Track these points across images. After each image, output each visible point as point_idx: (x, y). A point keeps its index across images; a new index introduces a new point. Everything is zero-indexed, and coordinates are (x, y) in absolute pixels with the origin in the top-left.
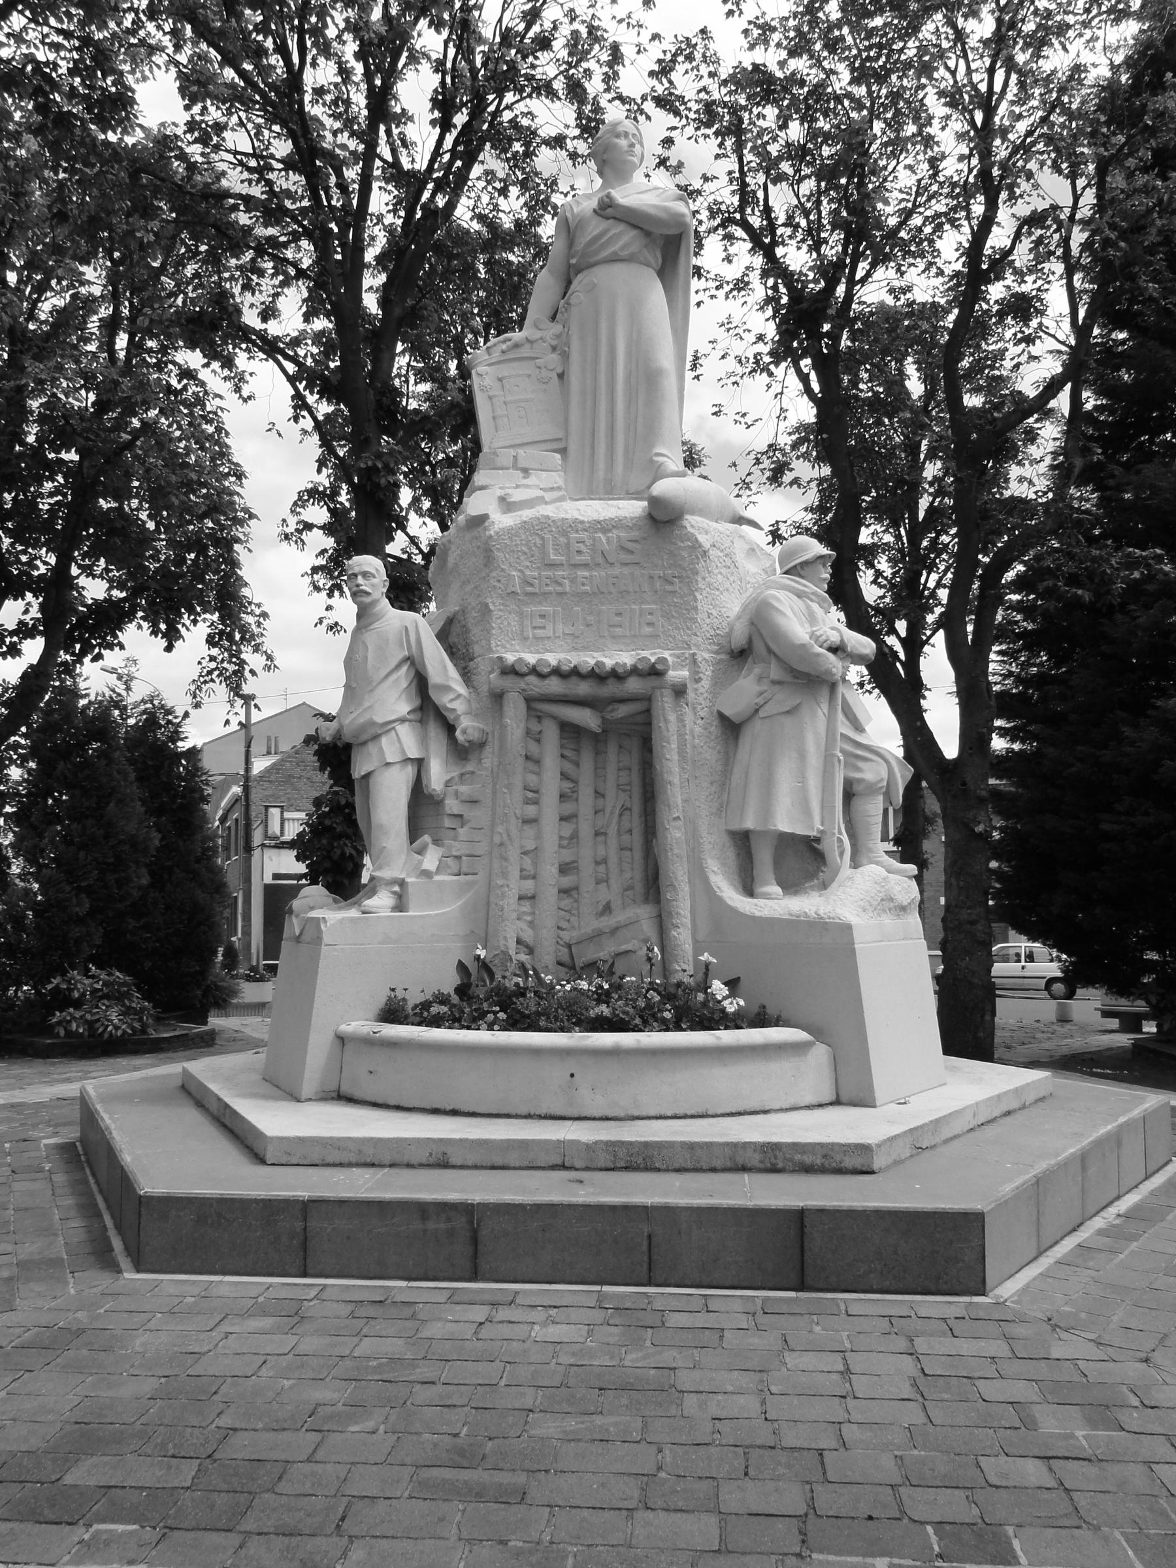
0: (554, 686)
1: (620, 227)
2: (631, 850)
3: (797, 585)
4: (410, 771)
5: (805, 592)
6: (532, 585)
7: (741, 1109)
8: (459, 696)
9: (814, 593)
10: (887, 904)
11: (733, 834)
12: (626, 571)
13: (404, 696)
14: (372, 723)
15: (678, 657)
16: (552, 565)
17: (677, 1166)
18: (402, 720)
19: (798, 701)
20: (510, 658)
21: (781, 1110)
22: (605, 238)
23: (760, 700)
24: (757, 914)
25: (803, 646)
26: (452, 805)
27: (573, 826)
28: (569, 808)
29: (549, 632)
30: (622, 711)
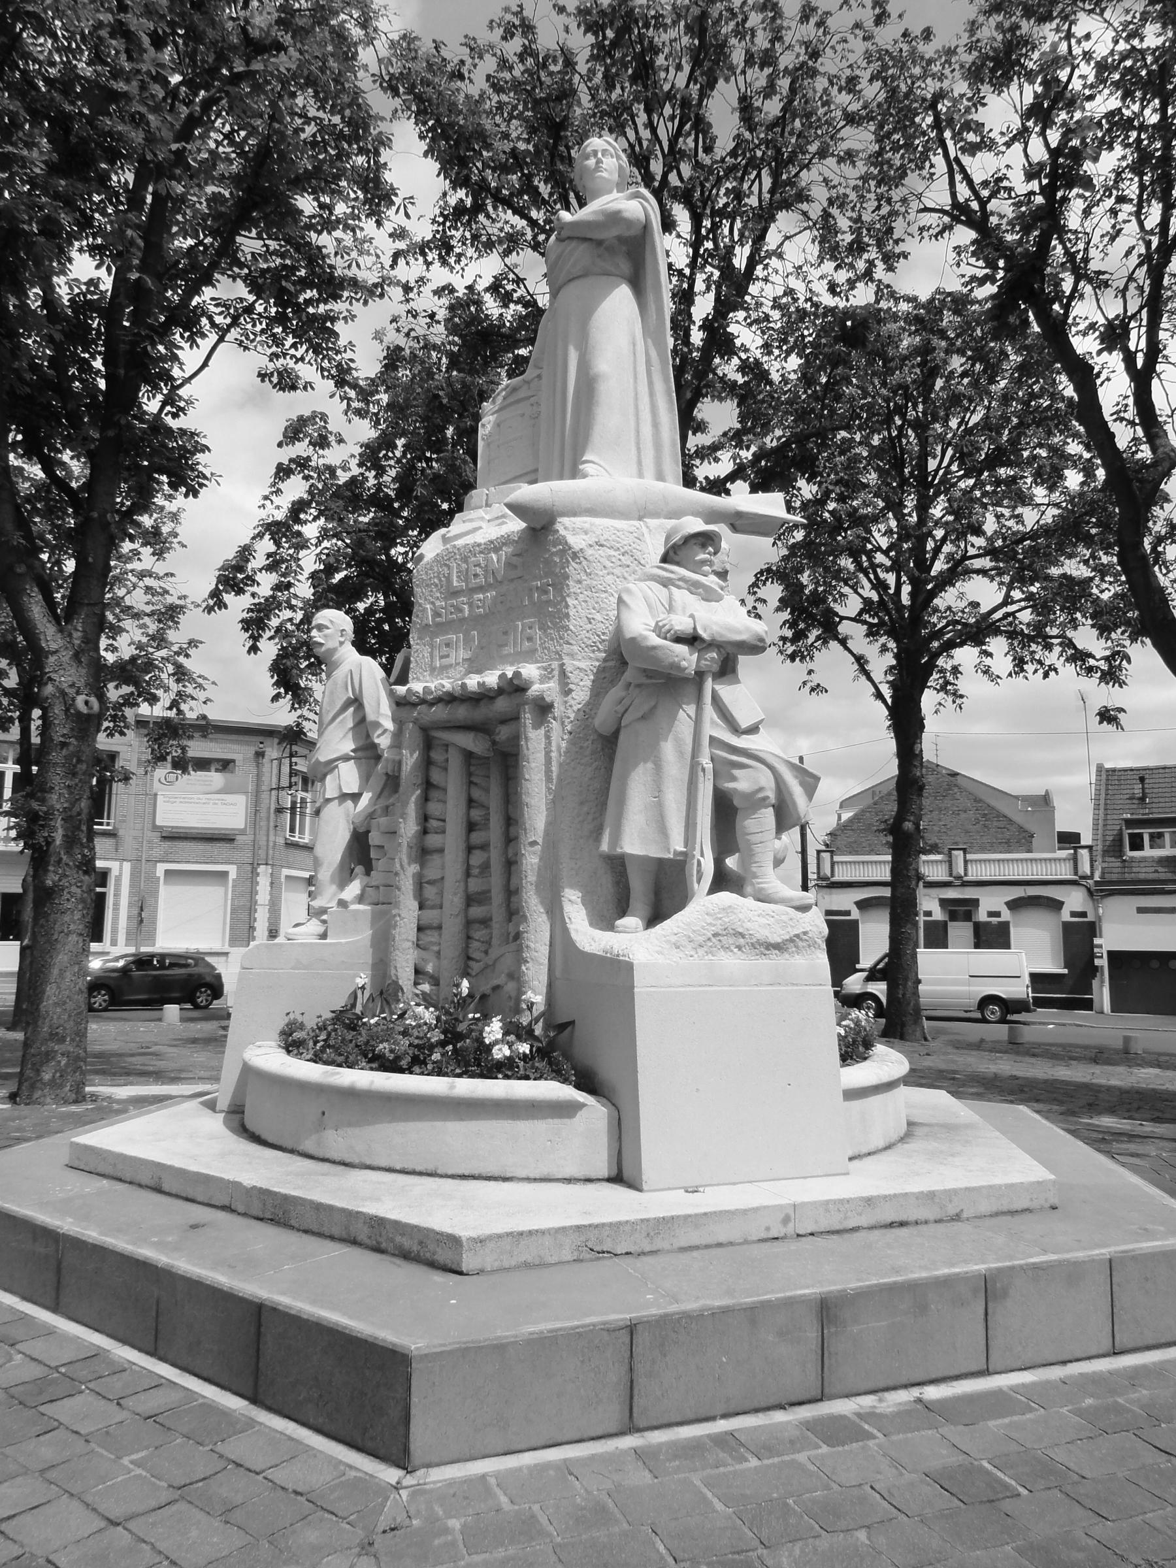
0: (439, 713)
5: (670, 579)
7: (476, 1172)
8: (385, 731)
9: (682, 579)
13: (350, 735)
15: (545, 669)
16: (456, 593)
17: (306, 1227)
18: (346, 758)
19: (653, 703)
21: (528, 1179)
23: (621, 709)
29: (452, 660)
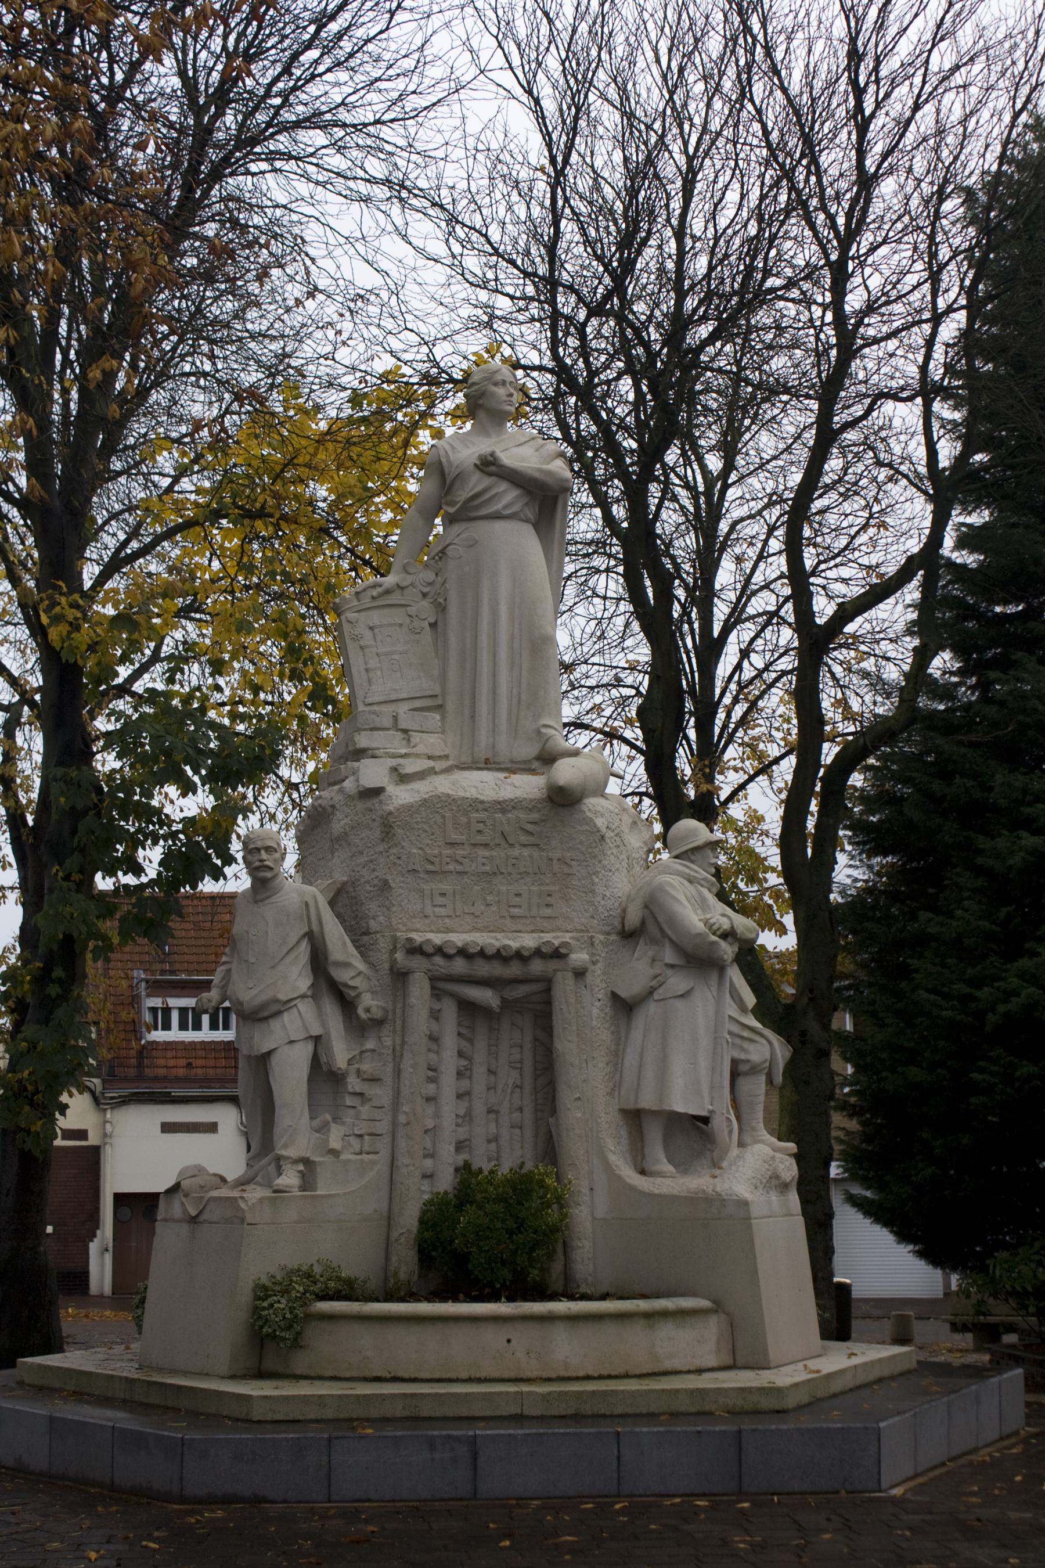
0: (459, 966)
1: (503, 486)
2: (521, 1128)
3: (687, 871)
4: (310, 1047)
6: (432, 863)
10: (774, 1182)
11: (624, 1112)
12: (526, 852)
14: (277, 1001)
16: (452, 844)
18: (303, 997)
20: (418, 938)
22: (487, 496)
23: (654, 983)
24: (657, 1192)
25: (699, 935)
26: (353, 1083)
27: (466, 1104)
28: (465, 1084)
30: (522, 990)
